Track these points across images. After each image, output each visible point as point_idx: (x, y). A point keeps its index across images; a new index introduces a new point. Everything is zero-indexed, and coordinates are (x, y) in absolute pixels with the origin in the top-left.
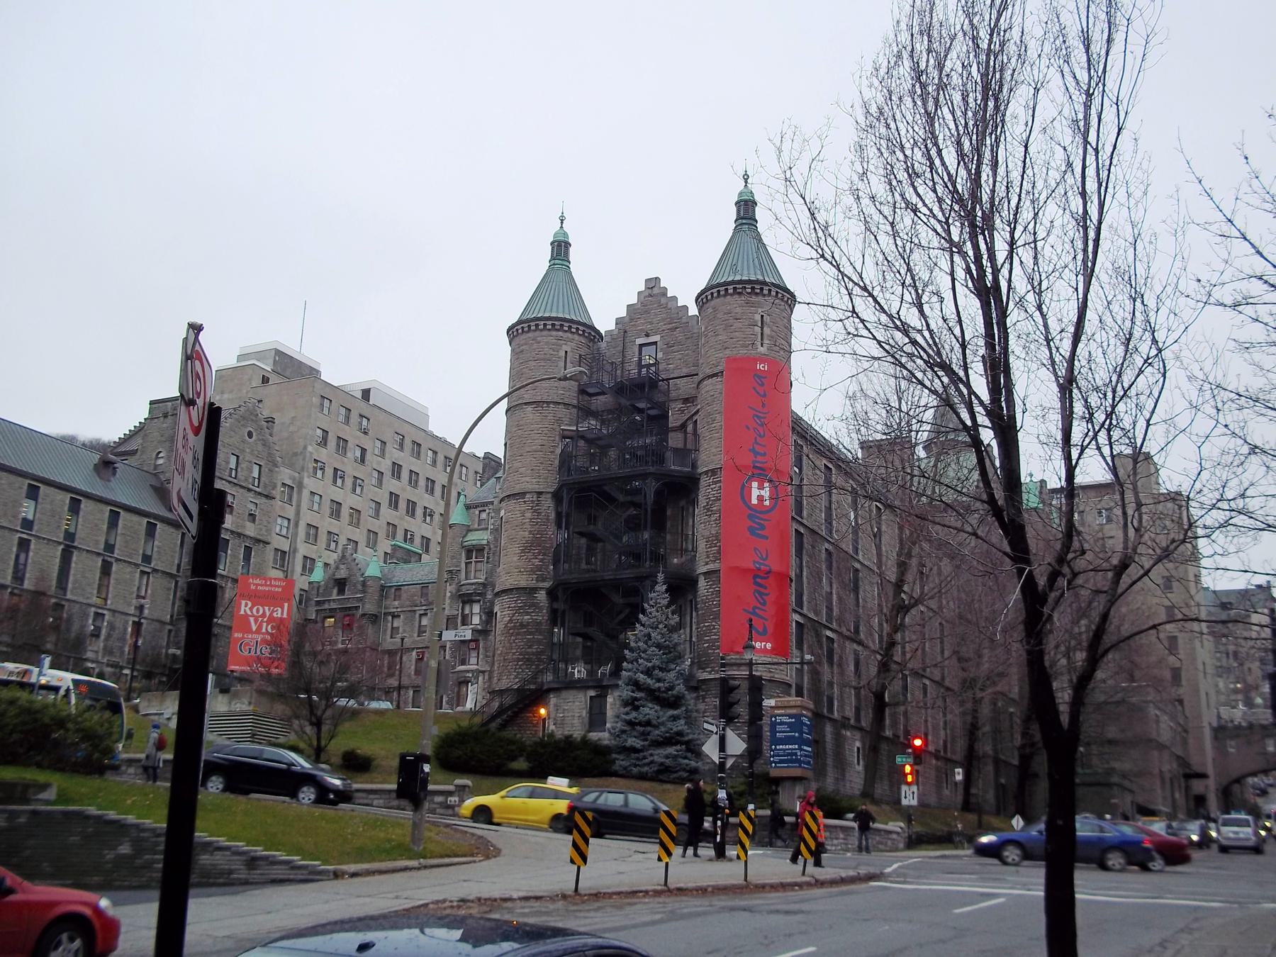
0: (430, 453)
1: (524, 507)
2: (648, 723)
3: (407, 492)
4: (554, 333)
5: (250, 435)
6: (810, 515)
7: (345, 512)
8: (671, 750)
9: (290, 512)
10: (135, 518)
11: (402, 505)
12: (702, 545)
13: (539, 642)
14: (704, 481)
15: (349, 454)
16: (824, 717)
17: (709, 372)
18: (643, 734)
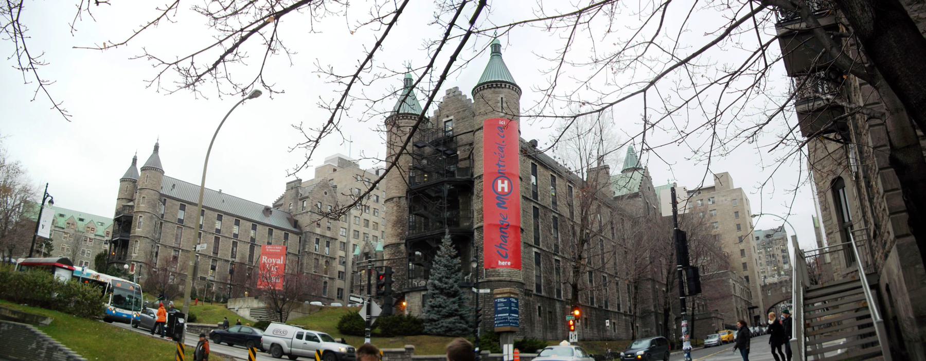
1: (393, 205)
2: (440, 306)
6: (542, 199)
7: (371, 224)
8: (452, 319)
9: (346, 225)
10: (279, 231)
13: (402, 270)
14: (476, 182)
16: (554, 299)
18: (438, 312)
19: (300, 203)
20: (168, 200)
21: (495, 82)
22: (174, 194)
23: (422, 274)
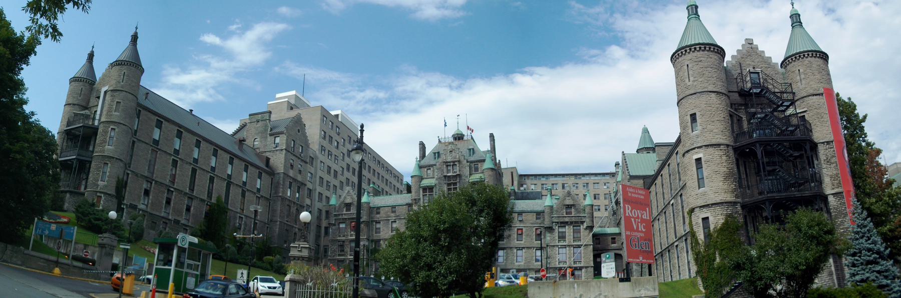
1: (721, 153)
19: (270, 139)
21: (687, 46)
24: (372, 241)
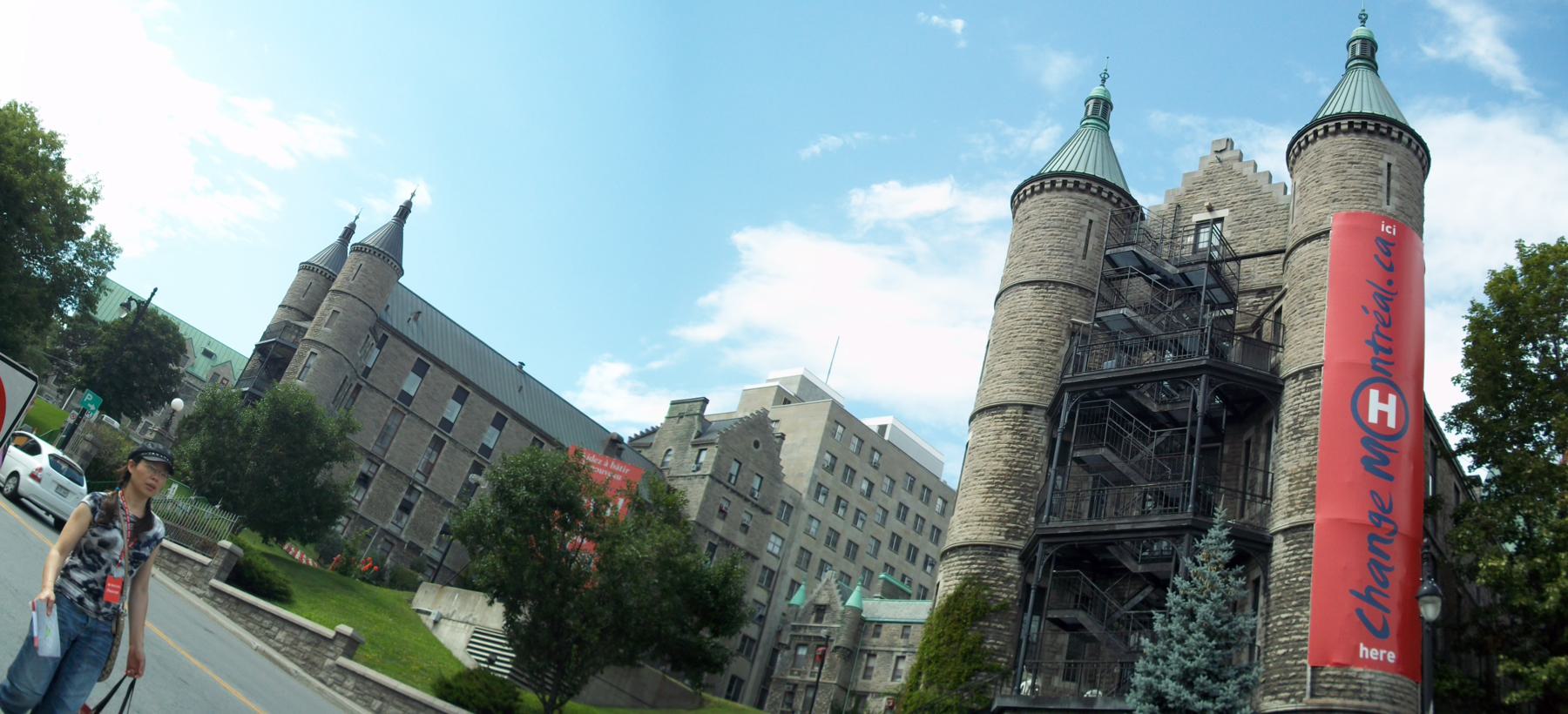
0: (940, 502)
1: (1002, 425)
3: (910, 537)
4: (1077, 195)
5: (756, 444)
7: (842, 543)
11: (904, 549)
12: (1282, 488)
14: (1290, 390)
15: (855, 485)
17: (1304, 234)
20: (391, 340)
21: (1372, 117)
22: (411, 332)
23: (1061, 659)
24: (853, 693)
